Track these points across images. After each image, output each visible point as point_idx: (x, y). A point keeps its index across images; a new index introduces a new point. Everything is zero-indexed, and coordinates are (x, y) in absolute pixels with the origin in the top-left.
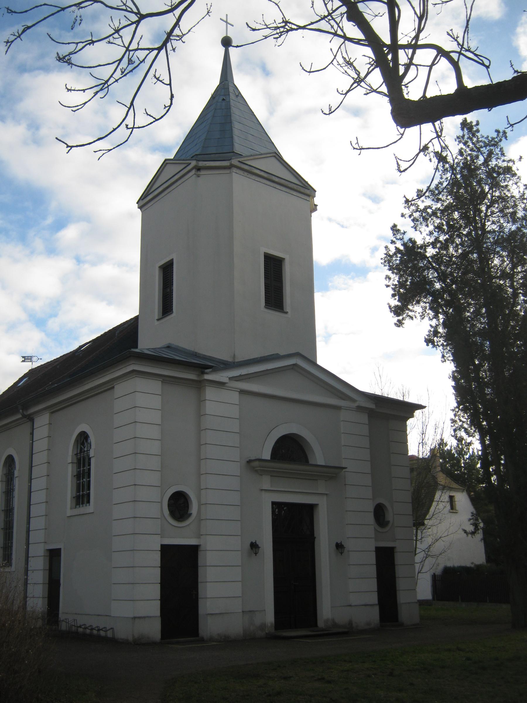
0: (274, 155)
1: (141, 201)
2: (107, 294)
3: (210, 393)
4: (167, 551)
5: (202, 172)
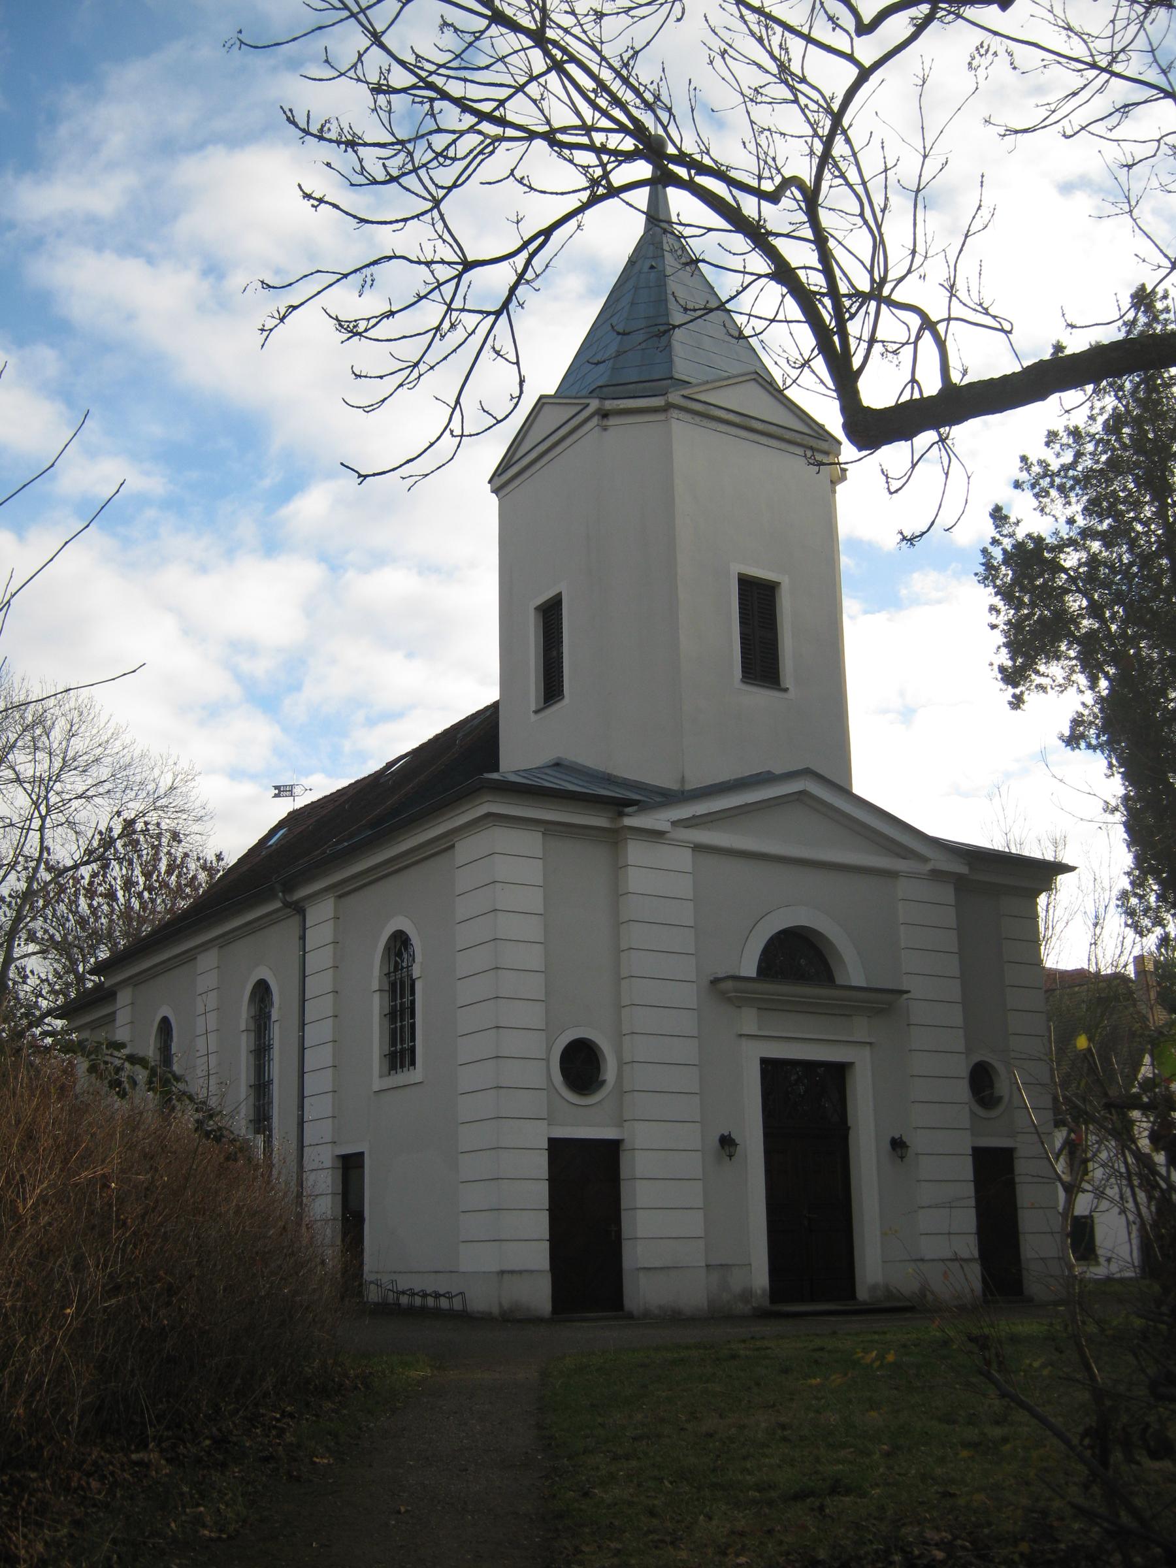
0: (755, 376)
1: (496, 478)
2: (438, 665)
3: (636, 852)
4: (560, 1151)
5: (612, 421)
